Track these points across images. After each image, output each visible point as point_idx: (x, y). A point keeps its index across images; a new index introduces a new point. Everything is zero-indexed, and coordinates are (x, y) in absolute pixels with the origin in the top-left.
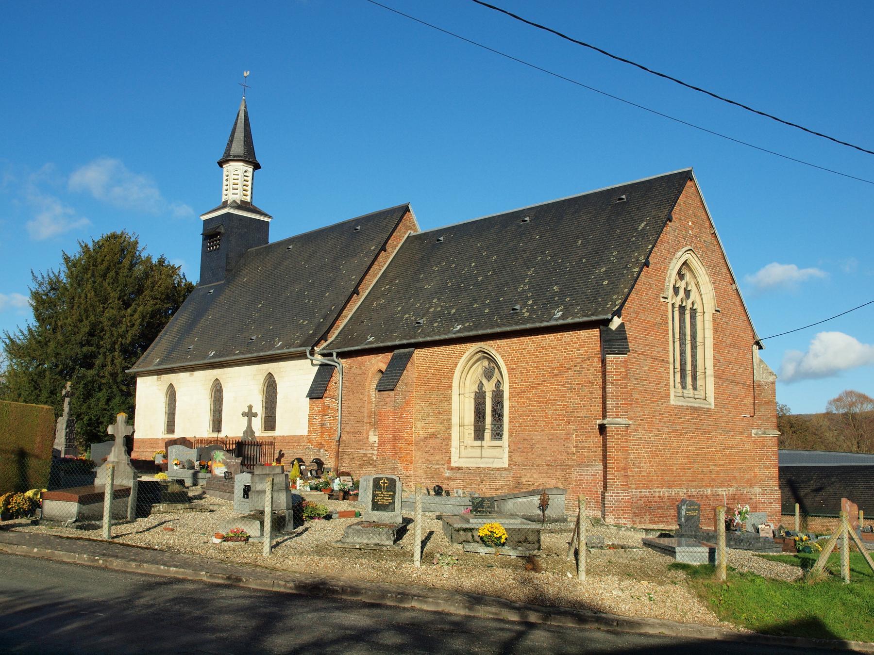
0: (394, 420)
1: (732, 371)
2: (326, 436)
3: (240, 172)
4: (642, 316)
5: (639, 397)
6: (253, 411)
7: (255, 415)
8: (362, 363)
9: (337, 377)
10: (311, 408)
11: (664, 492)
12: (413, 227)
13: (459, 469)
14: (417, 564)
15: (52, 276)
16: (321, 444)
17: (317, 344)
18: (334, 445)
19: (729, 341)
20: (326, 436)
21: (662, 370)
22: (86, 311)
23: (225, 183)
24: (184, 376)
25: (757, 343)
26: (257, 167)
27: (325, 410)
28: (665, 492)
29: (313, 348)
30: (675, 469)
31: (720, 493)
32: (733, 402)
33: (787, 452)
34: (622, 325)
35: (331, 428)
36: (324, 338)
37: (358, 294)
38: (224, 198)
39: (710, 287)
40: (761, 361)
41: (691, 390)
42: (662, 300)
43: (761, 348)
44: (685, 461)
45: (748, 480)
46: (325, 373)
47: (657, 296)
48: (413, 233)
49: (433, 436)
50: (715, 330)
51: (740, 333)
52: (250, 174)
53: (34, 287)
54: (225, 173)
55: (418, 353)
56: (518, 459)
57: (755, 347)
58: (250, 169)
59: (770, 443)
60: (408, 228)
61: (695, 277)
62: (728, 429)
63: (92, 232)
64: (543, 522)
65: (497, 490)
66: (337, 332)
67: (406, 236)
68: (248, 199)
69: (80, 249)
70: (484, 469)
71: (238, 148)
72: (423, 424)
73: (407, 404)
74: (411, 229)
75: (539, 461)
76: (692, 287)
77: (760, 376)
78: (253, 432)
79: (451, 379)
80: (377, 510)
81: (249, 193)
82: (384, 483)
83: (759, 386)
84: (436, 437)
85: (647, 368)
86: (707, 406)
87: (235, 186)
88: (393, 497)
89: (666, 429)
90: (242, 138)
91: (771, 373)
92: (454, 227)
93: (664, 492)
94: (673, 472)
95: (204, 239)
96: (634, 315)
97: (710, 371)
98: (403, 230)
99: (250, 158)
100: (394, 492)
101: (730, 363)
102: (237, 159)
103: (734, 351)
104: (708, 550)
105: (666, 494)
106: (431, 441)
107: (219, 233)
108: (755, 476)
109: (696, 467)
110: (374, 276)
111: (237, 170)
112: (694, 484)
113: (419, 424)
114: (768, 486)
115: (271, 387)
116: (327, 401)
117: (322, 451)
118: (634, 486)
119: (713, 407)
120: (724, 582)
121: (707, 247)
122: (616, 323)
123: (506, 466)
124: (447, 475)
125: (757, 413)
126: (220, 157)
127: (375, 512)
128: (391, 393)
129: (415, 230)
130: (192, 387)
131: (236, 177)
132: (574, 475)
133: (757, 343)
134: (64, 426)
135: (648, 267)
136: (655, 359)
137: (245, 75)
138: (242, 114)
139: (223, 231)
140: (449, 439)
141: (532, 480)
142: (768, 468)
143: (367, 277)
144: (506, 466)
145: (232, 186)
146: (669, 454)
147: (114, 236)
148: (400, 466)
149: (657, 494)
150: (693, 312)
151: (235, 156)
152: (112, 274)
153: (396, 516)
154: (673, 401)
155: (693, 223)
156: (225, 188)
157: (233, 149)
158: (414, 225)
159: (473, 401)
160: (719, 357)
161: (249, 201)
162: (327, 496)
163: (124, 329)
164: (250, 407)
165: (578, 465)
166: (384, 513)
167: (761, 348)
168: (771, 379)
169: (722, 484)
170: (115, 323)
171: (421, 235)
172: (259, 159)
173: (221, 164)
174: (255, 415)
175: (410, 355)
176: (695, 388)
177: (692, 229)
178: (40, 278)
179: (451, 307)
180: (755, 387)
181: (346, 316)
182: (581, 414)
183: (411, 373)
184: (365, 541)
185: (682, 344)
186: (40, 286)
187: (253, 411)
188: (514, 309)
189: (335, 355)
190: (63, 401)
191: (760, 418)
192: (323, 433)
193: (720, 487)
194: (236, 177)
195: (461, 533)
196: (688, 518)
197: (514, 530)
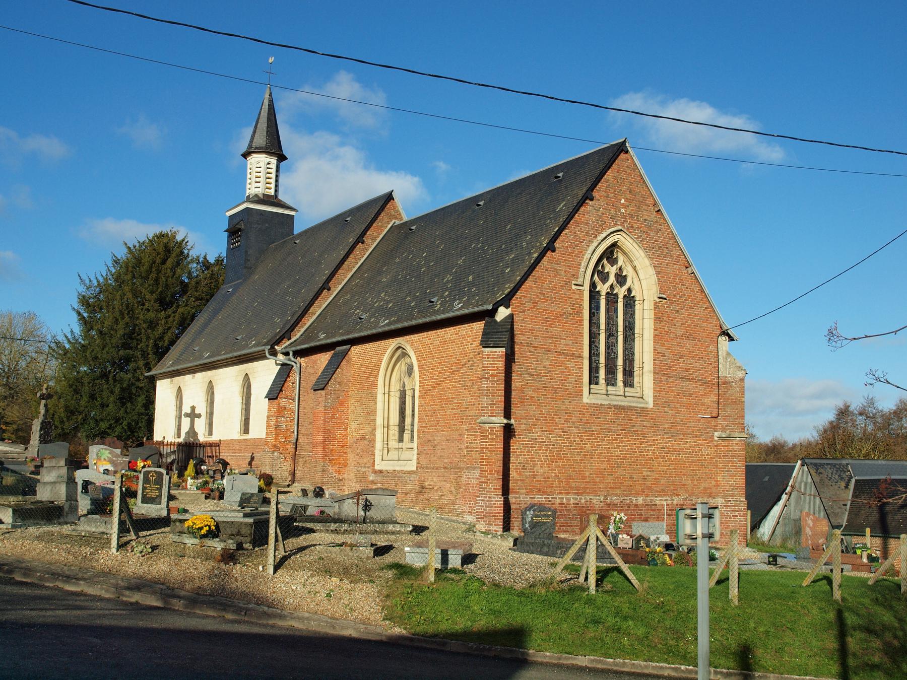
0: (325, 421)
1: (683, 366)
2: (281, 438)
3: (262, 165)
4: (542, 306)
5: (534, 394)
6: (197, 412)
7: (199, 416)
8: (315, 362)
9: (295, 377)
10: (269, 410)
11: (569, 499)
12: (398, 216)
13: (381, 472)
14: (114, 550)
15: (101, 280)
16: (275, 446)
17: (278, 342)
18: (291, 448)
19: (679, 332)
20: (281, 438)
21: (572, 364)
22: (122, 313)
23: (249, 176)
24: (188, 377)
25: (725, 333)
26: (282, 158)
27: (281, 411)
28: (572, 499)
29: (272, 347)
30: (587, 474)
31: (658, 502)
32: (684, 400)
33: (883, 462)
34: (511, 316)
35: (287, 430)
36: (287, 334)
37: (329, 289)
38: (248, 192)
39: (651, 271)
40: (728, 354)
41: (622, 387)
42: (574, 287)
43: (731, 339)
44: (603, 466)
45: (706, 489)
46: (285, 371)
47: (567, 283)
48: (398, 222)
49: (363, 438)
50: (658, 319)
51: (694, 323)
52: (273, 165)
53: (82, 289)
54: (249, 166)
55: (355, 350)
56: (424, 462)
57: (723, 340)
58: (274, 161)
59: (736, 448)
60: (391, 217)
61: (631, 261)
62: (673, 431)
63: (139, 232)
64: (364, 522)
65: (406, 494)
66: (303, 330)
67: (389, 226)
68: (272, 192)
69: (126, 251)
70: (399, 472)
71: (261, 140)
72: (356, 426)
73: (341, 404)
74: (396, 218)
75: (439, 464)
76: (628, 271)
77: (726, 371)
78: (196, 434)
79: (377, 376)
80: (147, 503)
81: (273, 186)
82: (153, 476)
83: (725, 383)
84: (365, 439)
85: (548, 363)
86: (642, 405)
87: (258, 180)
88: (160, 489)
89: (575, 430)
90: (265, 129)
91: (740, 368)
92: (427, 215)
93: (569, 499)
94: (584, 477)
95: (229, 236)
96: (529, 305)
97: (649, 366)
98: (386, 220)
99: (274, 148)
100: (161, 487)
101: (681, 357)
102: (259, 151)
103: (689, 345)
104: (440, 551)
105: (572, 501)
106: (362, 443)
107: (240, 230)
108: (717, 485)
109: (620, 472)
110: (349, 270)
111: (260, 162)
112: (618, 491)
113: (353, 425)
114: (733, 496)
115: (210, 389)
116: (283, 402)
117: (276, 454)
118: (524, 491)
119: (651, 405)
120: (432, 584)
121: (649, 227)
122: (502, 313)
123: (414, 469)
124: (371, 478)
125: (722, 413)
126: (244, 149)
127: (145, 505)
128: (323, 392)
129: (401, 219)
130: (193, 386)
131: (258, 170)
132: (464, 479)
133: (725, 333)
134: (39, 428)
135: (554, 251)
136: (561, 353)
137: (270, 61)
138: (266, 103)
139: (243, 227)
140: (373, 441)
141: (432, 483)
142: (733, 476)
143: (340, 271)
144: (414, 469)
145: (254, 179)
146: (578, 458)
147: (162, 235)
148: (330, 469)
149: (558, 501)
150: (630, 301)
151: (256, 148)
152: (153, 275)
153: (162, 509)
154: (586, 399)
155: (626, 200)
156: (249, 181)
157: (255, 140)
158: (400, 214)
159: (398, 400)
160: (661, 349)
161: (273, 194)
162: (203, 495)
163: (161, 330)
164: (193, 408)
165: (467, 468)
166: (150, 505)
167: (731, 339)
168: (740, 374)
169: (662, 493)
170: (152, 325)
171: (406, 222)
172: (285, 152)
173: (245, 155)
174: (199, 416)
175: (346, 353)
176: (628, 383)
177: (626, 207)
178: (87, 282)
179: (390, 301)
180: (720, 384)
181: (314, 313)
182: (472, 413)
183: (345, 371)
184: (94, 530)
185: (594, 337)
186: (88, 288)
187: (197, 412)
188: (431, 302)
189: (291, 354)
190: (39, 404)
191: (725, 418)
192: (277, 435)
193: (660, 496)
194: (258, 170)
195: (178, 524)
196: (534, 525)
197: (228, 522)
